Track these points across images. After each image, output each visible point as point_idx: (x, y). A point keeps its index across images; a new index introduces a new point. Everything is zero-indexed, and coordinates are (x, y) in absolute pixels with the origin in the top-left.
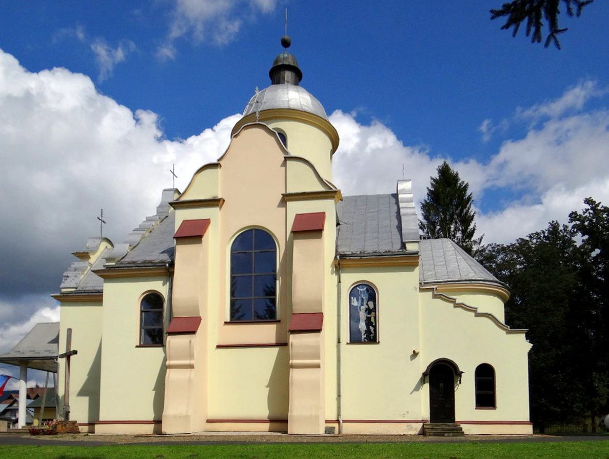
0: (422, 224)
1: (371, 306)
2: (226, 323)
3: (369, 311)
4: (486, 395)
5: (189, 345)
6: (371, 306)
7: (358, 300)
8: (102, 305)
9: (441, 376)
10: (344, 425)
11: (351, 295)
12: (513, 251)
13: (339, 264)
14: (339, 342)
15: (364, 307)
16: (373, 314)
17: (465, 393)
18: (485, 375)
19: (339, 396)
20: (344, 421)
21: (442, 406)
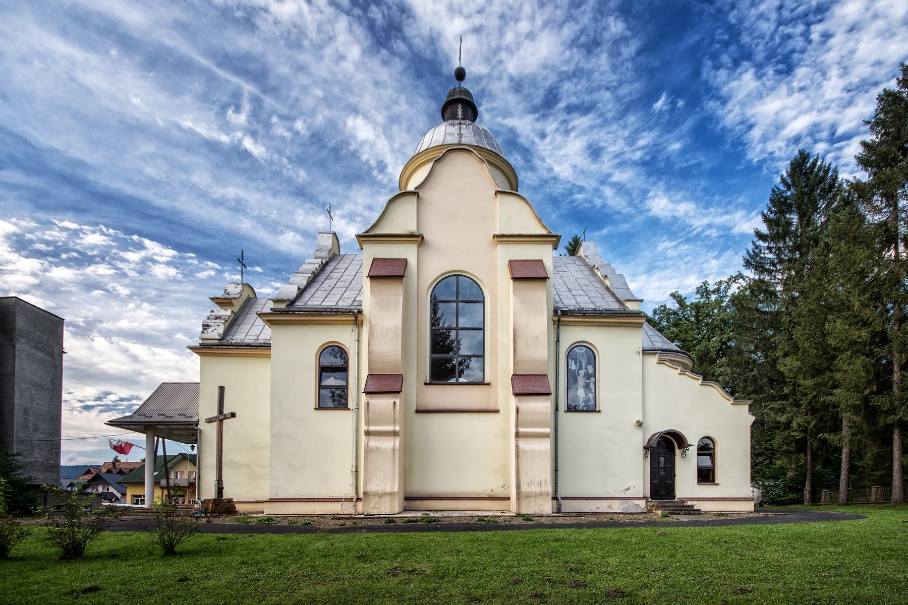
0: (351, 92)
1: (591, 371)
2: (426, 384)
3: (588, 376)
4: (706, 476)
5: (392, 407)
6: (591, 371)
7: (576, 364)
8: (268, 356)
9: (664, 448)
10: (563, 502)
11: (568, 357)
12: (247, 214)
13: (559, 320)
14: (557, 409)
15: (582, 372)
16: (593, 379)
17: (686, 470)
18: (706, 449)
19: (556, 470)
20: (563, 498)
21: (662, 486)
